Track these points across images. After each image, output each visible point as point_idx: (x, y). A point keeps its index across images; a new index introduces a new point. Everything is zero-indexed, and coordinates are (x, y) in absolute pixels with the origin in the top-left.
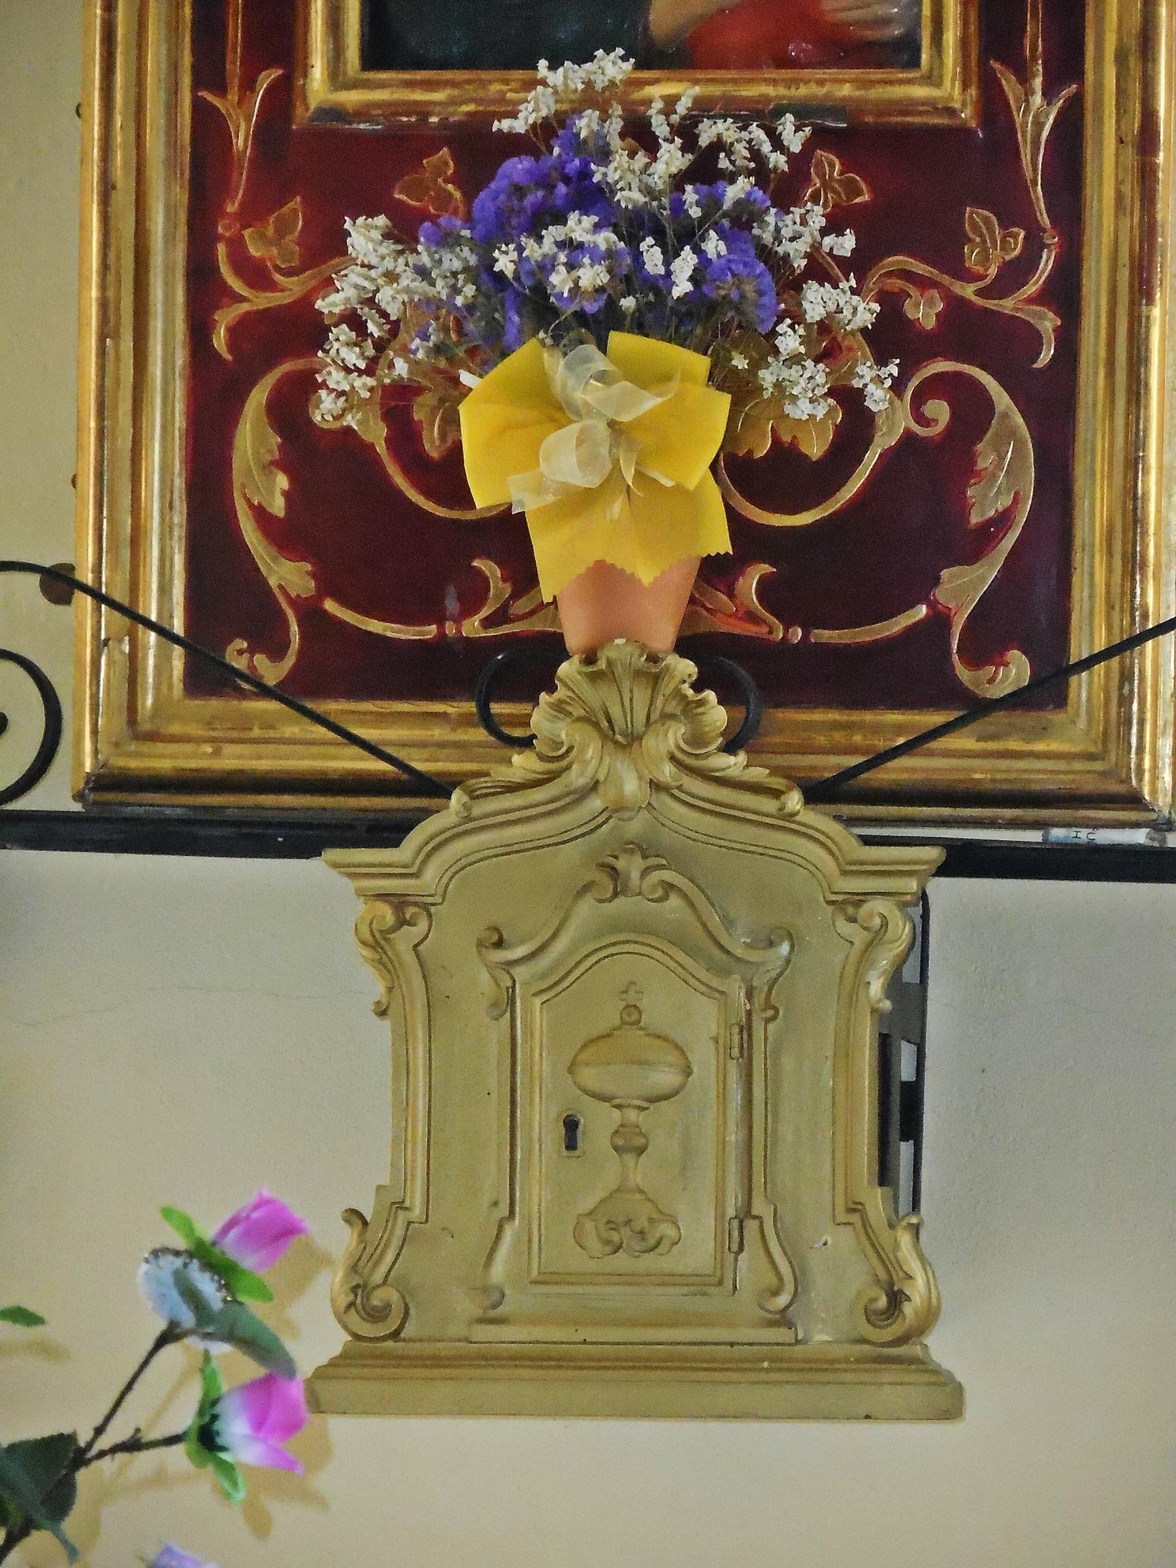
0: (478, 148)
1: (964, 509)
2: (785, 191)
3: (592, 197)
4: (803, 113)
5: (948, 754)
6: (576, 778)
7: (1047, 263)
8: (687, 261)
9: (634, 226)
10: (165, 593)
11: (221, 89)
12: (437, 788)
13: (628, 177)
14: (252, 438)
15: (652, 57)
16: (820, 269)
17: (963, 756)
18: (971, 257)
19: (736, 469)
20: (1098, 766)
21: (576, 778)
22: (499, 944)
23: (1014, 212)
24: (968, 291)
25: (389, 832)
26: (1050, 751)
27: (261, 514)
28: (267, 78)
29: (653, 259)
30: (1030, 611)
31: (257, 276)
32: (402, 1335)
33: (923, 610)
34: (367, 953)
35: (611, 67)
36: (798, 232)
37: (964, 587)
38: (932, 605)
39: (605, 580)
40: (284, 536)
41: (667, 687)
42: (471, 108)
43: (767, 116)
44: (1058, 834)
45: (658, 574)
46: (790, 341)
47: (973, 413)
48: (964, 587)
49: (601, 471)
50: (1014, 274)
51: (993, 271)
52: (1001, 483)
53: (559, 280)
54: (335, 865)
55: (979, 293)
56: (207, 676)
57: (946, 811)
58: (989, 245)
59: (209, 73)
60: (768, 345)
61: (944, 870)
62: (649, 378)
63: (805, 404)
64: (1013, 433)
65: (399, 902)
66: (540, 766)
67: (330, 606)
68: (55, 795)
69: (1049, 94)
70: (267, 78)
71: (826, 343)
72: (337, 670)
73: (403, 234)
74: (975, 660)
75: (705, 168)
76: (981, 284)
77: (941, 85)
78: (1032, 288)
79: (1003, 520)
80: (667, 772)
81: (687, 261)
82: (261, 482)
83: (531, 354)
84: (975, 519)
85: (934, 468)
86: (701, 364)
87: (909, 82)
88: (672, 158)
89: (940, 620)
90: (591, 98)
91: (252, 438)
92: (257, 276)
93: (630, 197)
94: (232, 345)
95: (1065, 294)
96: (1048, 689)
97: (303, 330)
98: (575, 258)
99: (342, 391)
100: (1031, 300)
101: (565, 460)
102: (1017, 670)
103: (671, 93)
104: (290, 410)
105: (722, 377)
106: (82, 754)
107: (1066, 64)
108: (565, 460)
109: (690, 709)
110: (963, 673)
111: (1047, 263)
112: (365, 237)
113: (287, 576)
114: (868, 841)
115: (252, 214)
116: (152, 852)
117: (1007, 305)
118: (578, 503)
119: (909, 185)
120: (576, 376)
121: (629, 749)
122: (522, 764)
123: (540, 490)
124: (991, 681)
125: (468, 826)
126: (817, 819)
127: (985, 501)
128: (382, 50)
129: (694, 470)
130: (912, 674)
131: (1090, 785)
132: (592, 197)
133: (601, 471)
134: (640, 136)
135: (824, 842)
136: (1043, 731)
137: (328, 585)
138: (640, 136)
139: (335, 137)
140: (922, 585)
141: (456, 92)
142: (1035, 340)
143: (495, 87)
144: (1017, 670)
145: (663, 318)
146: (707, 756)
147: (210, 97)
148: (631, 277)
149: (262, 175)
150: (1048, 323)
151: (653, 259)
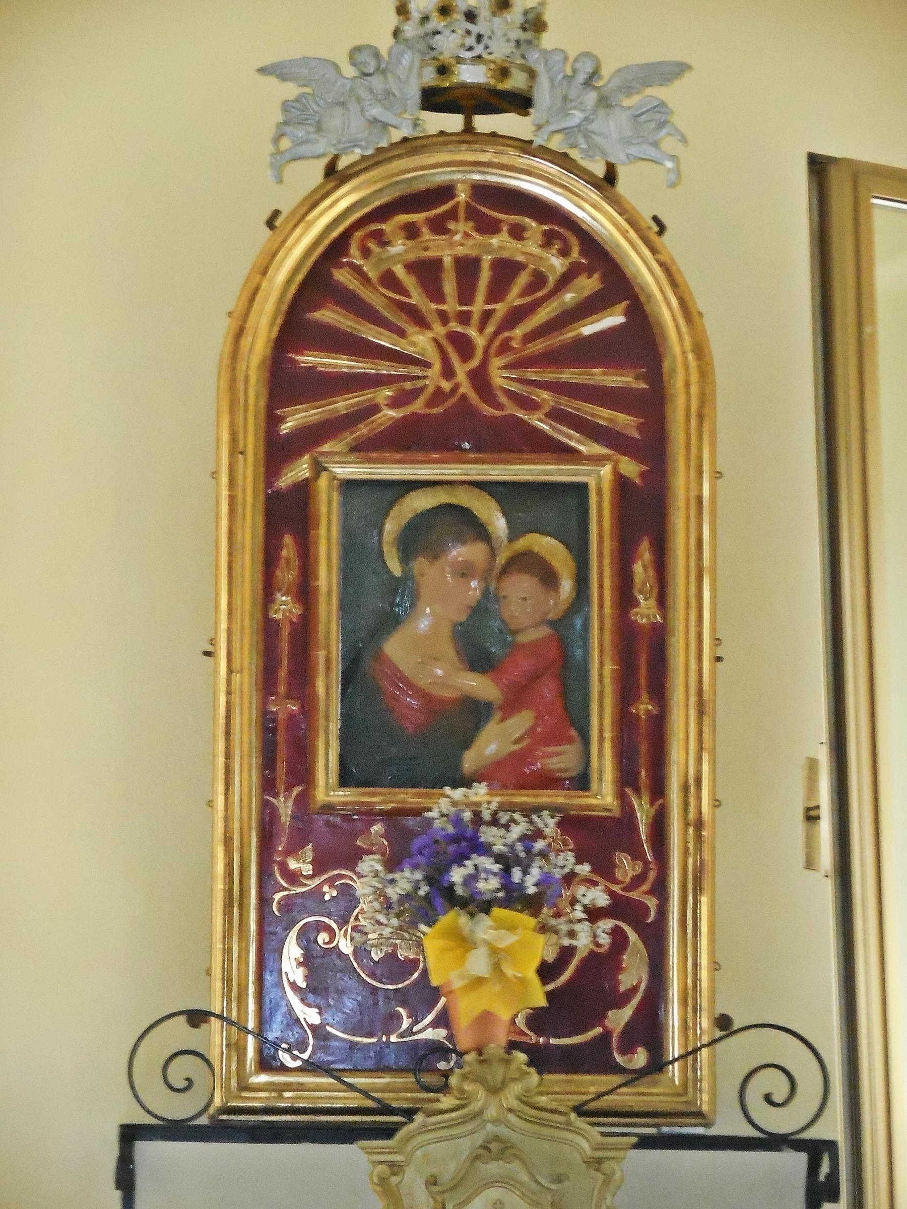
1: (617, 983)
3: (484, 849)
4: (554, 810)
5: (620, 1094)
6: (476, 1106)
7: (652, 875)
11: (276, 796)
12: (409, 1113)
18: (619, 875)
20: (684, 1099)
21: (476, 1106)
22: (435, 1184)
23: (637, 854)
24: (616, 888)
25: (387, 1132)
27: (293, 985)
28: (297, 790)
30: (648, 1029)
33: (598, 1030)
34: (378, 1189)
37: (619, 1019)
38: (604, 1027)
39: (485, 1019)
41: (513, 1066)
42: (393, 805)
44: (665, 1130)
47: (619, 940)
48: (619, 1019)
50: (638, 880)
51: (628, 880)
52: (633, 973)
54: (363, 1148)
55: (623, 889)
57: (615, 1120)
58: (626, 867)
59: (268, 786)
61: (636, 1146)
64: (639, 951)
65: (391, 1165)
66: (458, 1102)
69: (652, 803)
70: (297, 790)
74: (624, 1051)
76: (623, 885)
77: (604, 796)
78: (646, 887)
79: (634, 990)
80: (515, 1104)
83: (453, 918)
84: (622, 988)
85: (603, 964)
86: (532, 922)
87: (587, 797)
89: (607, 1035)
92: (293, 878)
94: (279, 911)
95: (660, 889)
100: (646, 893)
102: (640, 1058)
107: (658, 790)
110: (618, 1058)
111: (652, 875)
114: (604, 1134)
115: (293, 850)
116: (184, 1140)
117: (633, 895)
122: (447, 1101)
123: (462, 977)
124: (630, 1061)
125: (424, 1129)
126: (580, 1123)
127: (626, 981)
128: (345, 780)
130: (594, 1058)
131: (681, 1108)
132: (484, 849)
135: (586, 1137)
136: (655, 1084)
140: (599, 1018)
141: (382, 798)
142: (647, 909)
143: (402, 796)
144: (640, 1058)
146: (531, 1097)
147: (271, 799)
150: (652, 903)
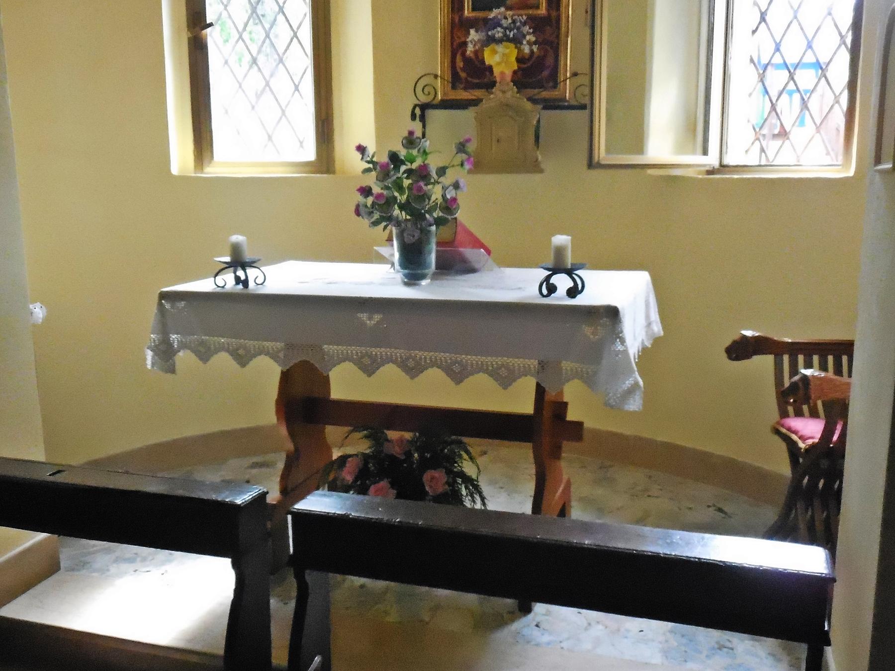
0: (486, 21)
2: (525, 24)
3: (501, 26)
8: (512, 33)
9: (505, 29)
10: (448, 76)
13: (505, 23)
14: (459, 58)
15: (509, 8)
16: (529, 33)
17: (545, 94)
19: (519, 60)
26: (555, 94)
29: (508, 32)
31: (459, 38)
32: (289, 489)
35: (502, 9)
36: (526, 29)
37: (546, 73)
39: (502, 73)
40: (463, 69)
43: (522, 15)
45: (509, 73)
46: (525, 42)
47: (546, 51)
48: (546, 73)
49: (501, 60)
52: (550, 61)
53: (497, 36)
56: (454, 87)
60: (521, 43)
62: (507, 48)
63: (526, 49)
67: (469, 79)
68: (435, 102)
71: (529, 43)
72: (468, 86)
73: (477, 31)
75: (514, 22)
81: (512, 33)
82: (460, 64)
83: (493, 46)
88: (510, 21)
90: (499, 13)
91: (459, 58)
92: (459, 38)
93: (505, 25)
96: (555, 86)
97: (465, 44)
98: (498, 33)
99: (470, 48)
101: (497, 58)
102: (551, 84)
103: (509, 13)
104: (463, 54)
105: (516, 47)
106: (439, 97)
108: (497, 58)
109: (512, 89)
112: (472, 31)
113: (463, 75)
118: (499, 64)
119: (537, 24)
120: (500, 48)
121: (505, 93)
128: (474, 9)
129: (513, 59)
130: (541, 86)
132: (501, 26)
133: (501, 60)
134: (506, 18)
135: (528, 105)
137: (468, 75)
138: (506, 18)
139: (468, 19)
145: (509, 40)
148: (505, 35)
149: (457, 27)
151: (508, 32)
